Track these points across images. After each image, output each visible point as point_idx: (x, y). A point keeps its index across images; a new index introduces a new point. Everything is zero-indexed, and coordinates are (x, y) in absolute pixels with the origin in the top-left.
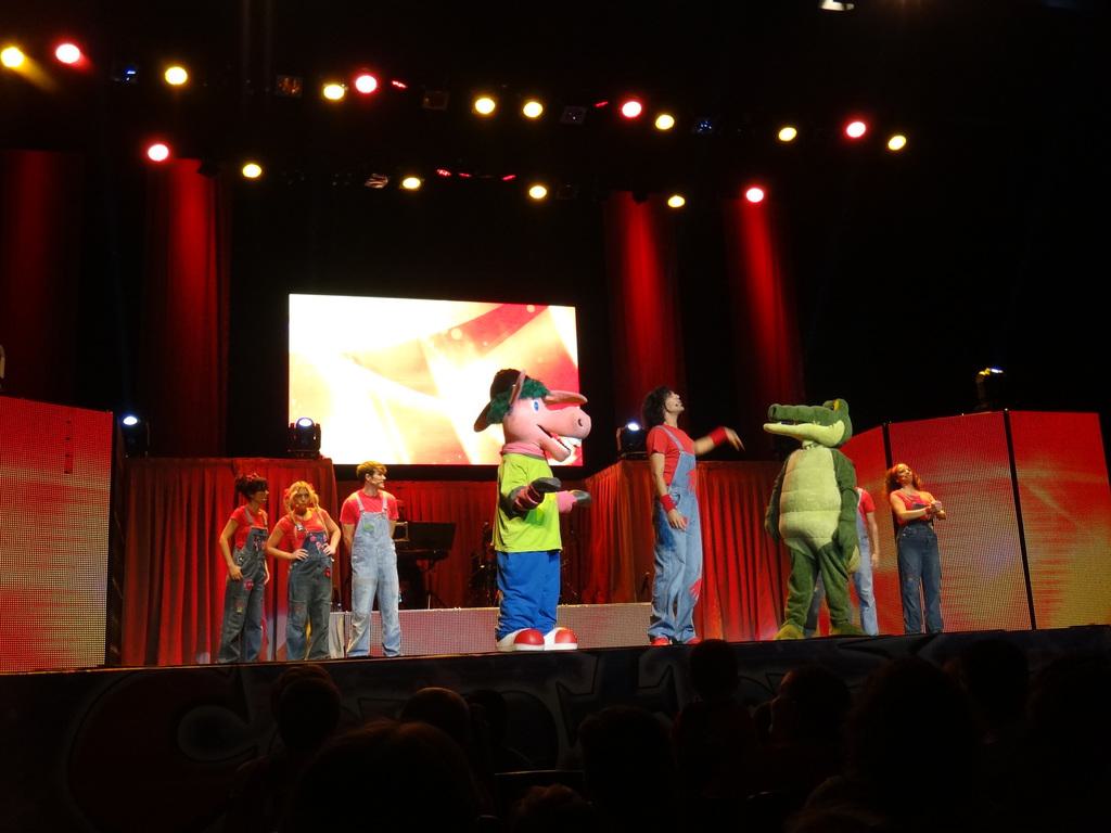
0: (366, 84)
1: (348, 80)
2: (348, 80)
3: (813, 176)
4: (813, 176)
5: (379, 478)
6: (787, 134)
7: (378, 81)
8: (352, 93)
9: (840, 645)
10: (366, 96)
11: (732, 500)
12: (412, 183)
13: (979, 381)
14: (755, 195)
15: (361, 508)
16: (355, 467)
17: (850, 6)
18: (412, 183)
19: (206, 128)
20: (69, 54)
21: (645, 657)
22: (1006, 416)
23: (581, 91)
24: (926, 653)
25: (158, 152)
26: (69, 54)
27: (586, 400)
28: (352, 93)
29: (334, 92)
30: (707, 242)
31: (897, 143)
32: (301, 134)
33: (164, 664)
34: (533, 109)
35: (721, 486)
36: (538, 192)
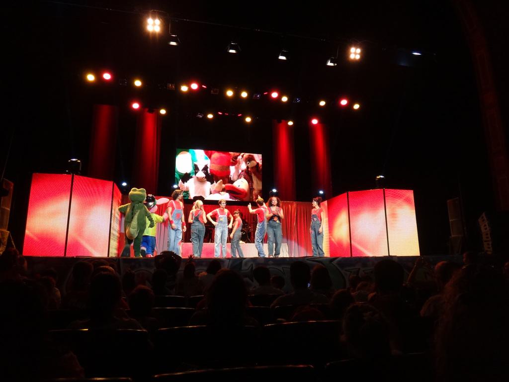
0: (194, 86)
1: (189, 85)
2: (189, 85)
3: (331, 115)
4: (331, 115)
5: (223, 205)
6: (322, 103)
7: (276, 98)
8: (190, 89)
9: (307, 259)
10: (195, 90)
11: (304, 214)
12: (210, 116)
13: (377, 179)
14: (315, 122)
15: (219, 214)
16: (218, 201)
17: (336, 64)
18: (210, 116)
19: (150, 98)
20: (107, 76)
21: (244, 261)
22: (384, 190)
23: (259, 87)
24: (335, 262)
25: (136, 106)
26: (107, 76)
27: (221, 180)
28: (190, 89)
29: (184, 89)
30: (302, 134)
31: (356, 107)
32: (174, 100)
33: (281, 256)
34: (244, 95)
35: (304, 209)
36: (248, 120)
